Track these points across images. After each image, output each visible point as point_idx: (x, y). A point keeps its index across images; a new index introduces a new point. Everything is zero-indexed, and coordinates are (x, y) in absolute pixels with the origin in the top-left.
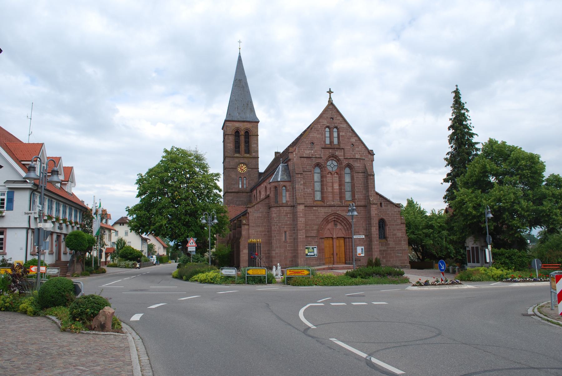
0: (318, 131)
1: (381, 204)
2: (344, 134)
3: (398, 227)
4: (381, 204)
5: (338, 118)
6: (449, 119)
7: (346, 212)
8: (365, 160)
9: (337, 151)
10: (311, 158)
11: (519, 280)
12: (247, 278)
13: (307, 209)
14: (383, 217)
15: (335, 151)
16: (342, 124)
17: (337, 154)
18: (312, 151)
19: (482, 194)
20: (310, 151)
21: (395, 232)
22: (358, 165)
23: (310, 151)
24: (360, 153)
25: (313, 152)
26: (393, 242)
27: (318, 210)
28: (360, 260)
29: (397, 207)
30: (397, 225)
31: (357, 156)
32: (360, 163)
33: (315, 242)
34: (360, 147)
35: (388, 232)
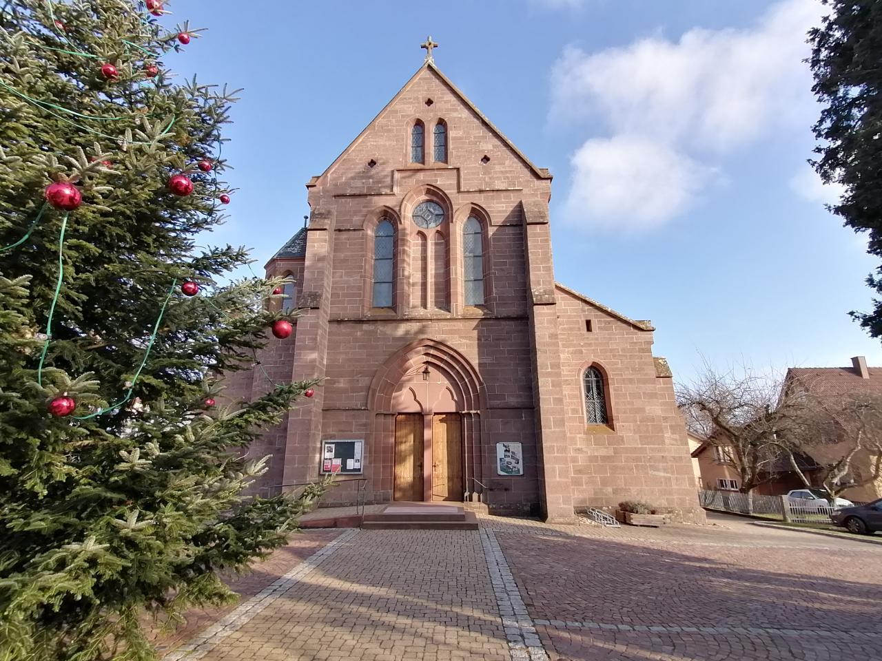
0: (389, 131)
1: (588, 323)
2: (461, 133)
3: (649, 388)
4: (588, 323)
5: (445, 99)
6: (822, 19)
7: (460, 337)
8: (523, 191)
9: (441, 175)
10: (366, 195)
11: (78, 147)
12: (667, 384)
13: (344, 331)
14: (597, 360)
15: (435, 175)
16: (456, 110)
17: (438, 183)
18: (371, 180)
19: (121, 569)
20: (364, 181)
21: (638, 404)
22: (503, 207)
23: (364, 181)
24: (508, 178)
25: (373, 182)
26: (635, 433)
27: (375, 332)
28: (506, 490)
29: (642, 330)
30: (645, 382)
31: (500, 185)
32: (507, 203)
33: (361, 425)
34: (507, 162)
35: (616, 403)
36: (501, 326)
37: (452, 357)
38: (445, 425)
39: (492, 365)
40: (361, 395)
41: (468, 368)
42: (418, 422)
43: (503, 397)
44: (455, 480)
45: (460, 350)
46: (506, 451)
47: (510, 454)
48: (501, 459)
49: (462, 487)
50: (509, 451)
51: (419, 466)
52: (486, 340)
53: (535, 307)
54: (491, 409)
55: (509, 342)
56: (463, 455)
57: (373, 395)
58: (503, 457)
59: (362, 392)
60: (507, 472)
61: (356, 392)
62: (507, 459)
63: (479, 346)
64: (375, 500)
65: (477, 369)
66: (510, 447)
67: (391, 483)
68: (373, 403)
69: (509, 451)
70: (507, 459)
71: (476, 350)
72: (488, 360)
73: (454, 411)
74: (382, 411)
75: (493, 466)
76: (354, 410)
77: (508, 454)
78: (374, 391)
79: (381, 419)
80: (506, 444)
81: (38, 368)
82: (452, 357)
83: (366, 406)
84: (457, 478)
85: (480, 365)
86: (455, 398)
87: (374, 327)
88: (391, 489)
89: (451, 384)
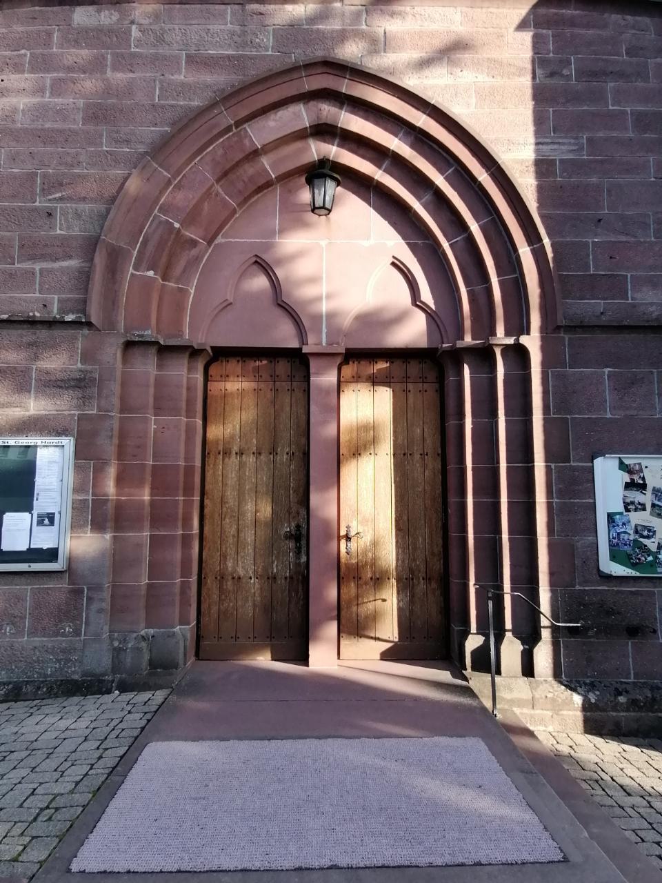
28: (633, 631)
36: (605, 26)
37: (421, 139)
38: (7, 514)
39: (572, 166)
40: (62, 270)
41: (483, 177)
42: (286, 385)
43: (615, 286)
44: (421, 587)
45: (457, 111)
46: (628, 486)
47: (647, 498)
48: (611, 517)
49: (446, 610)
50: (642, 487)
51: (289, 536)
52: (552, 75)
53: (31, 547)
54: (570, 329)
55: (640, 84)
56: (453, 499)
57: (113, 270)
58: (621, 508)
59: (70, 257)
60: (633, 566)
61: (43, 257)
62: (636, 518)
63: (541, 96)
64: (115, 669)
65: (527, 185)
66: (646, 473)
67: (184, 603)
68: (111, 300)
69: (642, 487)
70: (636, 518)
71: (524, 112)
72: (561, 151)
73: (423, 343)
74: (149, 334)
75: (582, 542)
76: (32, 323)
77: (637, 496)
78: (115, 258)
79: (147, 367)
80: (630, 460)
81: (183, 496)
82: (421, 139)
83: (84, 312)
84: (428, 579)
85: (543, 167)
86: (426, 295)
87: (115, 16)
88: (184, 621)
89: (413, 248)
